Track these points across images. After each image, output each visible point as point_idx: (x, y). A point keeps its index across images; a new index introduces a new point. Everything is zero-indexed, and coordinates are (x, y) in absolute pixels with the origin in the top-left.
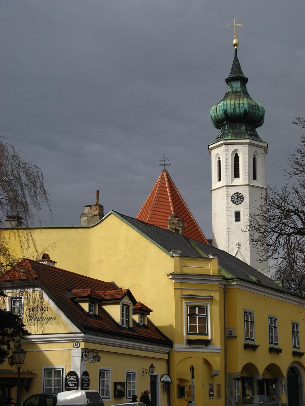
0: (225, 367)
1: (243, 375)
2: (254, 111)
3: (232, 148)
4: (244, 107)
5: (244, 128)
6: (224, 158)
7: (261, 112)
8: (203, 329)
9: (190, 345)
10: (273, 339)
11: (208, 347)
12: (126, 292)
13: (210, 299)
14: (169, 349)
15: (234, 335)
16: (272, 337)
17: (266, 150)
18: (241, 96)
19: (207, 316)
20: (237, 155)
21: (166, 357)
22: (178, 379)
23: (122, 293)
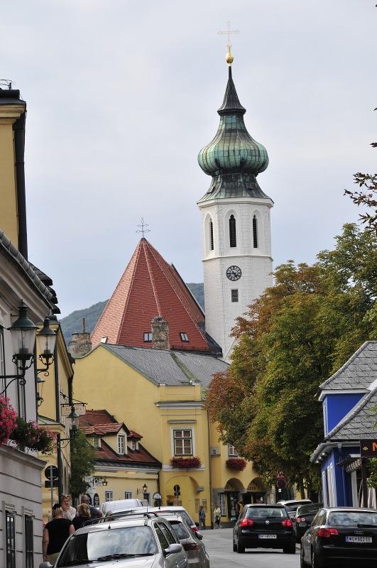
0: (210, 483)
1: (227, 490)
2: (254, 158)
3: (226, 210)
4: (240, 153)
5: (241, 180)
6: (217, 222)
13: (194, 422)
20: (232, 216)
21: (156, 477)
22: (168, 496)
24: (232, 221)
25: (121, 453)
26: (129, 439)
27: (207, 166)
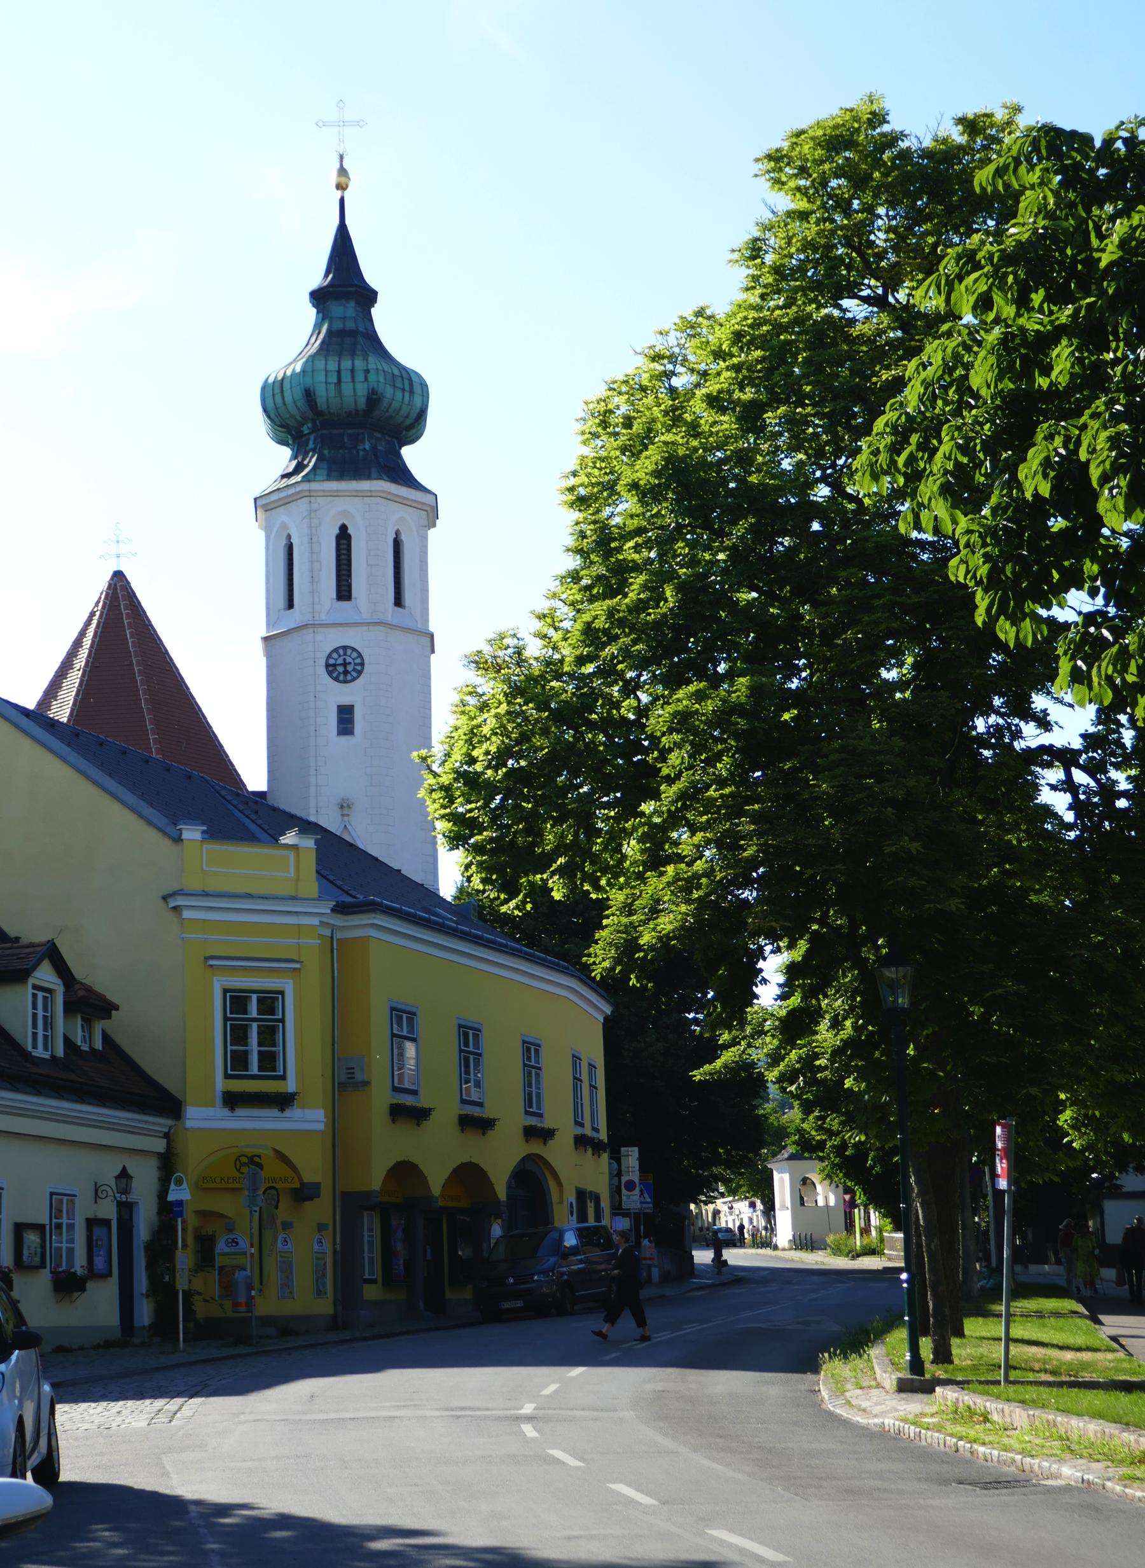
2: (399, 394)
4: (366, 379)
5: (367, 446)
7: (418, 400)
8: (269, 1061)
9: (232, 1110)
10: (532, 1101)
11: (287, 1113)
12: (44, 948)
14: (169, 1122)
15: (359, 1077)
16: (530, 1094)
17: (431, 514)
18: (359, 347)
19: (282, 1021)
20: (343, 528)
23: (34, 953)
24: (344, 538)
25: (40, 1052)
26: (70, 1008)
27: (282, 410)
